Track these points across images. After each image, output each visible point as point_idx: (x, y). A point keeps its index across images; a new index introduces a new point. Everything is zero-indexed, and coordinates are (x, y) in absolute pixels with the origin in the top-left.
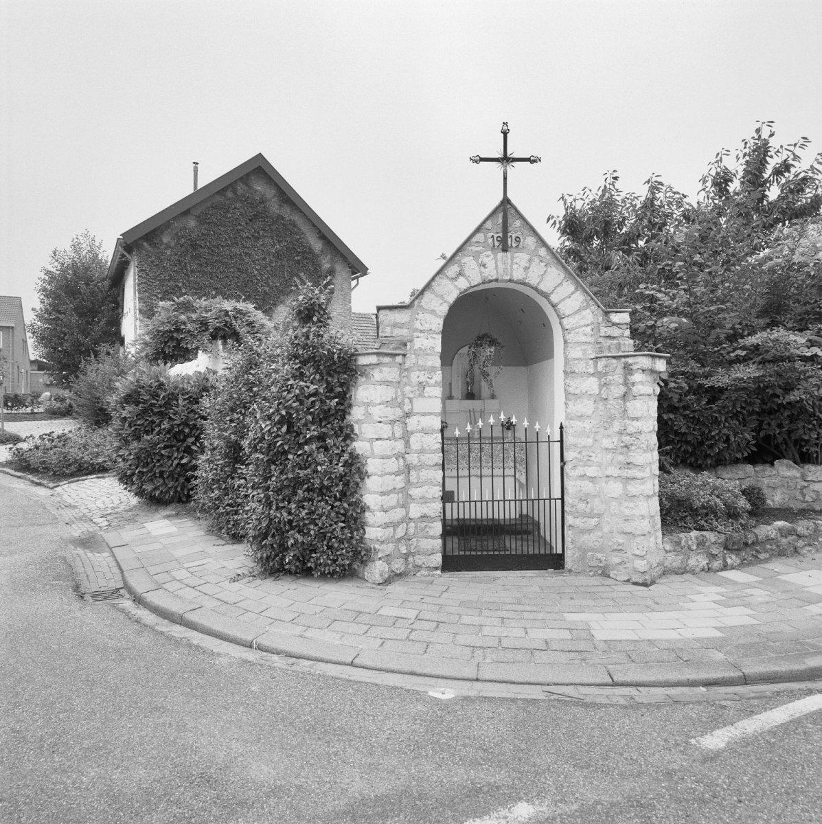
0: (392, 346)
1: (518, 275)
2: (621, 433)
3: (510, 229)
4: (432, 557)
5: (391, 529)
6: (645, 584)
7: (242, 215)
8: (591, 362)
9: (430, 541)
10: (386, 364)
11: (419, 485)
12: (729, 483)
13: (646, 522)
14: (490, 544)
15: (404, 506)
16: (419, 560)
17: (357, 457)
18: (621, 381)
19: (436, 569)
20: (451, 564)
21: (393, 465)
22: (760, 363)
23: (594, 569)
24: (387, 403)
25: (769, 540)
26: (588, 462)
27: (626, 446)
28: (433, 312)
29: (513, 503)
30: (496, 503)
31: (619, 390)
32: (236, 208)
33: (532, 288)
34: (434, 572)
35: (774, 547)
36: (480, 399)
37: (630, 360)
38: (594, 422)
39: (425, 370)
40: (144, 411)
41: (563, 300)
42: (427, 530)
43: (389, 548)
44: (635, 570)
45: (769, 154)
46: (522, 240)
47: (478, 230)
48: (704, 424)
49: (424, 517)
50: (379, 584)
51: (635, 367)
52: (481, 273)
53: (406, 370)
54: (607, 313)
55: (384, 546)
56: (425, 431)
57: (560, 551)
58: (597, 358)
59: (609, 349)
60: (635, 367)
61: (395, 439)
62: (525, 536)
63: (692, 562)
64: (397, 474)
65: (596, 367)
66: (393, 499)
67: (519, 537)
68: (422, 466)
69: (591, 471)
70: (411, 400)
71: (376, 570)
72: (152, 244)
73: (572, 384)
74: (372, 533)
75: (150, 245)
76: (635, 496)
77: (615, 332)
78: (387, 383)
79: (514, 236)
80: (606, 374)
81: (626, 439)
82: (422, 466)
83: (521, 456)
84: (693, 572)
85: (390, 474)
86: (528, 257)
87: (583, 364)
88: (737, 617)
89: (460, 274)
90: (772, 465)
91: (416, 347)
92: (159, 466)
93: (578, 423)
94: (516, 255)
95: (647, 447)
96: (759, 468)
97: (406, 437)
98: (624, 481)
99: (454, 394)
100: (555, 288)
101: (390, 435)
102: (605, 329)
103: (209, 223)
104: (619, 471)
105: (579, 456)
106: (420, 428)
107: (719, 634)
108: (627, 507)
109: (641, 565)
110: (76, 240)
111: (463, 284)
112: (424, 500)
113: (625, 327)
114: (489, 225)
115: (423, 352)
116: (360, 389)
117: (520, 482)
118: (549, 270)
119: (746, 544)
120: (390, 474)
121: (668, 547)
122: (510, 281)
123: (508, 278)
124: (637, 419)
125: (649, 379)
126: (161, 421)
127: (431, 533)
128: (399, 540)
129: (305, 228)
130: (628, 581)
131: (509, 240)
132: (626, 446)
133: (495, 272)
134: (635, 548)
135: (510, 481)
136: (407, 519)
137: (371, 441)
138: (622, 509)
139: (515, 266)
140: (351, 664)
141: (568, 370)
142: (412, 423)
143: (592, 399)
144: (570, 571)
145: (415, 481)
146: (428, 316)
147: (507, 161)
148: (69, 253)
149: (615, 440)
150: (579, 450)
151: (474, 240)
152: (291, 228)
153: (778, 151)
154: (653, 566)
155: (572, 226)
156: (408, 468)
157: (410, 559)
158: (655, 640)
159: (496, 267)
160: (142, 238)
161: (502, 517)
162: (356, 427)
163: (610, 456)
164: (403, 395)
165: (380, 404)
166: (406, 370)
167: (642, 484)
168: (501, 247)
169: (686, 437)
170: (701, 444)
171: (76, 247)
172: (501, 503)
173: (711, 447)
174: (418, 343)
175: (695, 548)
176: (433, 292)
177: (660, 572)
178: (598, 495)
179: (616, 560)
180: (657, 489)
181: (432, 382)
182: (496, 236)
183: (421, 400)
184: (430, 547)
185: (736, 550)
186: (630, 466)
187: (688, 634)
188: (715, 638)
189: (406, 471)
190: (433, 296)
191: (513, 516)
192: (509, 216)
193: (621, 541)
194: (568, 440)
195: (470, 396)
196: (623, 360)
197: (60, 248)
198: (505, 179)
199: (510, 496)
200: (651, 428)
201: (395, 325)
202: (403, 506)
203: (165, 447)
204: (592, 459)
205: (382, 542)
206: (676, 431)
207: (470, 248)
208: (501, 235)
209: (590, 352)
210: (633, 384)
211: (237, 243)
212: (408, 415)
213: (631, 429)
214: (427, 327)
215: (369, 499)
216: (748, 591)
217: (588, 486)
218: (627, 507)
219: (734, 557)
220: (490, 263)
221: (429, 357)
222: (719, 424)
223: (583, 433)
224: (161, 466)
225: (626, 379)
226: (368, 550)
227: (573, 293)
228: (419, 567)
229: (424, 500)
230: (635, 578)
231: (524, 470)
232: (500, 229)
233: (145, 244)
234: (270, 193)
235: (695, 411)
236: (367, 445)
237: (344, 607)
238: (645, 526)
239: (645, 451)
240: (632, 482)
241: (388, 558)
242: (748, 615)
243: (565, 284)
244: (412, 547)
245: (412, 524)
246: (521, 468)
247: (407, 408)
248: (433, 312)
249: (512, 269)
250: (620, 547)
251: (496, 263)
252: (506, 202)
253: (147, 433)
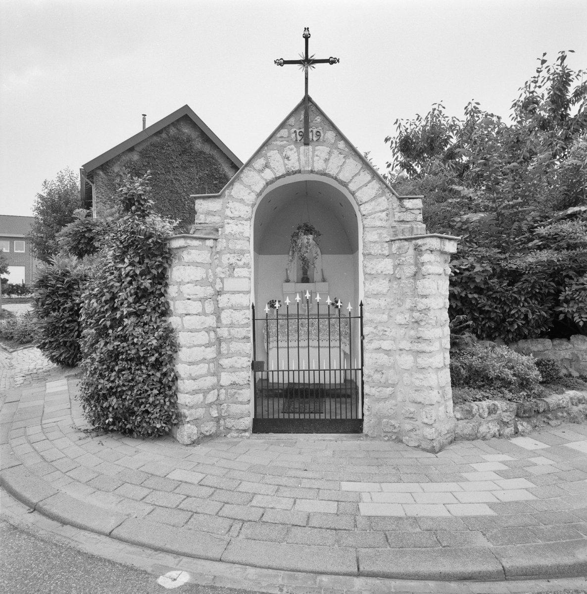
0: (204, 232)
1: (319, 166)
2: (412, 310)
3: (311, 124)
4: (241, 420)
5: (201, 396)
6: (433, 451)
7: (173, 150)
8: (386, 245)
9: (240, 406)
10: (195, 247)
11: (229, 356)
12: (499, 356)
13: (435, 392)
14: (312, 407)
15: (215, 374)
16: (230, 423)
17: (172, 331)
18: (412, 261)
19: (245, 431)
20: (261, 425)
21: (203, 338)
22: (556, 249)
23: (389, 435)
24: (196, 283)
25: (560, 408)
26: (383, 337)
27: (416, 322)
28: (241, 201)
29: (338, 372)
30: (322, 372)
31: (410, 270)
32: (169, 146)
33: (332, 177)
34: (243, 434)
35: (565, 414)
36: (313, 282)
37: (420, 242)
38: (389, 300)
39: (234, 253)
40: (53, 293)
41: (360, 188)
42: (237, 396)
43: (200, 412)
44: (425, 438)
45: (570, 78)
46: (322, 135)
47: (282, 126)
48: (505, 304)
49: (234, 384)
50: (187, 445)
51: (424, 248)
52: (285, 165)
53: (217, 253)
54: (400, 199)
55: (193, 411)
56: (234, 308)
57: (360, 417)
58: (392, 241)
59: (403, 232)
60: (424, 248)
61: (206, 315)
62: (343, 399)
63: (483, 429)
64: (207, 346)
65: (390, 248)
66: (203, 368)
67: (338, 400)
68: (232, 339)
69: (386, 345)
70: (222, 280)
71: (187, 431)
72: (106, 173)
73: (368, 264)
74: (183, 399)
75: (105, 173)
76: (424, 368)
77: (408, 217)
78: (197, 264)
79: (315, 131)
80: (400, 255)
81: (416, 315)
82: (232, 339)
83: (345, 329)
84: (484, 438)
85: (200, 346)
86: (328, 149)
87: (378, 246)
88: (516, 491)
89: (267, 166)
90: (569, 339)
91: (227, 232)
92: (63, 337)
93: (376, 301)
94: (317, 148)
95: (436, 322)
96: (557, 342)
97: (217, 313)
98: (414, 354)
99: (291, 278)
100: (353, 177)
101: (200, 310)
102: (399, 214)
103: (149, 157)
104: (410, 345)
105: (374, 331)
106: (229, 305)
107: (489, 512)
108: (417, 378)
109: (429, 432)
110: (60, 173)
111: (269, 175)
112: (233, 369)
113: (418, 212)
114: (292, 121)
115: (232, 237)
116: (174, 269)
117: (345, 353)
118: (347, 161)
119: (538, 412)
120: (200, 346)
121: (459, 416)
122: (312, 172)
123: (310, 169)
124: (425, 296)
125: (438, 259)
126: (65, 301)
127: (240, 399)
128: (210, 405)
129: (221, 161)
130: (418, 447)
131: (310, 134)
132: (416, 322)
133: (297, 164)
134: (424, 417)
135: (335, 352)
136: (219, 386)
137: (181, 316)
138: (414, 380)
139: (316, 158)
140: (109, 535)
141: (365, 252)
142: (223, 300)
143: (388, 279)
144: (367, 435)
145: (225, 352)
146: (237, 204)
147: (308, 63)
148: (55, 182)
149: (407, 316)
150: (376, 325)
151: (278, 135)
152: (209, 161)
153: (578, 75)
154: (443, 433)
155: (408, 147)
156: (219, 340)
157: (222, 422)
158: (420, 518)
159: (299, 160)
160: (98, 168)
161: (327, 382)
162: (171, 303)
163: (403, 331)
164: (215, 275)
165: (188, 283)
166: (217, 253)
167: (431, 357)
168: (302, 140)
169: (478, 311)
170: (504, 320)
171: (61, 180)
172: (306, 373)
173: (511, 324)
174: (228, 229)
175: (486, 415)
176: (242, 183)
177: (450, 439)
178: (392, 367)
179: (408, 427)
180: (448, 361)
181: (241, 263)
182: (298, 131)
183: (231, 280)
184: (239, 411)
185: (528, 417)
186: (420, 340)
187: (458, 511)
188: (485, 517)
189: (217, 342)
190: (242, 186)
191: (338, 382)
192: (310, 113)
193: (412, 410)
194: (366, 315)
195: (305, 279)
196: (414, 242)
197: (49, 180)
198: (307, 79)
199: (335, 365)
200: (442, 305)
201: (209, 213)
202: (214, 375)
203: (68, 322)
204: (387, 333)
205: (191, 407)
206: (480, 308)
207: (275, 143)
208: (303, 130)
209: (385, 235)
210: (423, 264)
211: (169, 172)
212: (219, 293)
213: (421, 306)
214: (236, 214)
215: (181, 368)
216: (533, 460)
217: (383, 359)
218: (417, 378)
219: (525, 424)
220: (293, 155)
221: (238, 242)
222: (518, 304)
223: (379, 310)
224: (65, 336)
225: (416, 259)
226: (178, 416)
227: (369, 182)
228: (229, 430)
229: (233, 369)
230: (424, 445)
231: (348, 342)
232: (302, 125)
233: (101, 173)
234: (194, 134)
235: (497, 292)
236: (178, 318)
237: (142, 469)
238: (435, 396)
239: (433, 327)
240: (421, 355)
241: (196, 421)
242: (526, 489)
243: (362, 173)
244: (223, 411)
245: (223, 391)
246: (345, 340)
247: (218, 287)
248: (241, 201)
249: (313, 161)
250: (411, 415)
251: (299, 155)
252: (307, 100)
253: (54, 310)
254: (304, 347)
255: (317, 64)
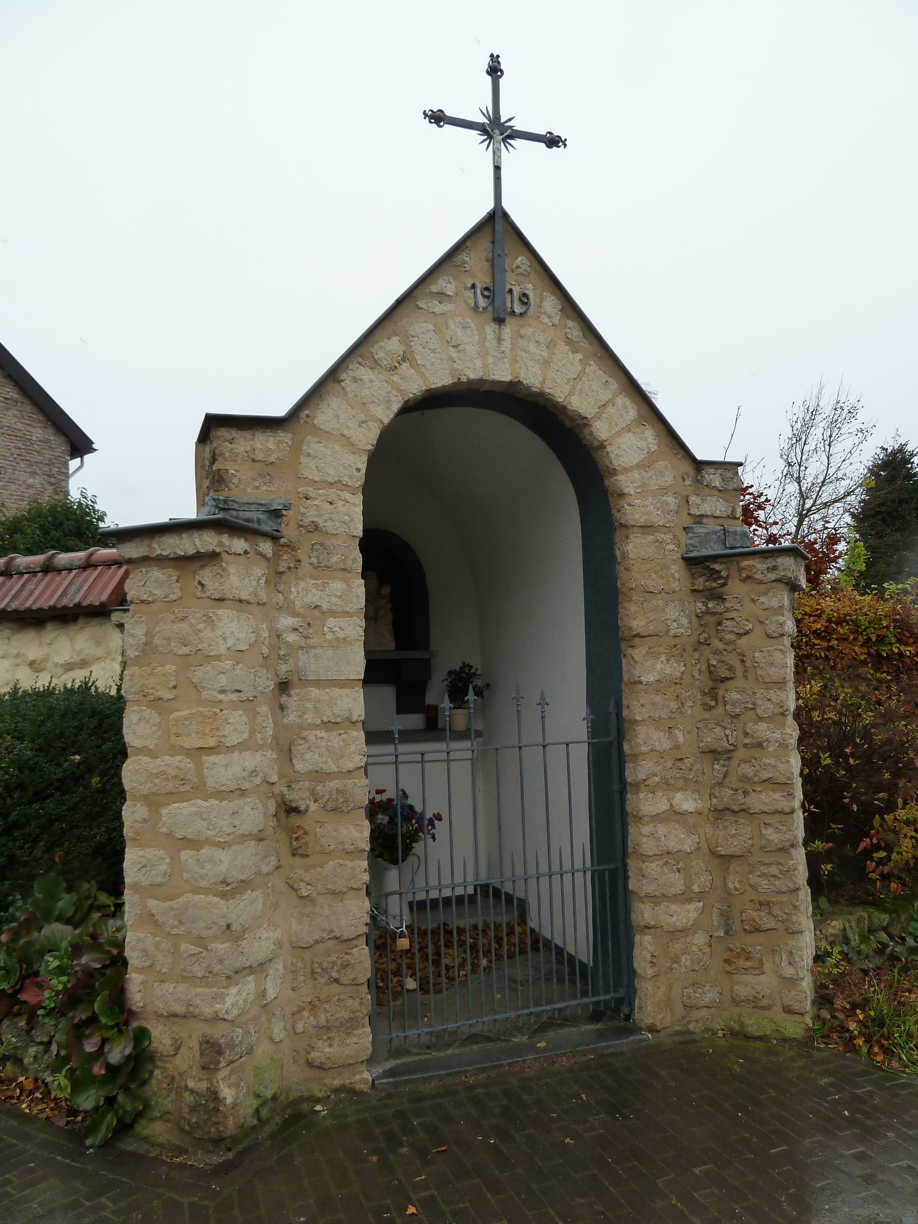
108: (763, 875)
218: (763, 875)
254: (578, 871)
255: (519, 140)
